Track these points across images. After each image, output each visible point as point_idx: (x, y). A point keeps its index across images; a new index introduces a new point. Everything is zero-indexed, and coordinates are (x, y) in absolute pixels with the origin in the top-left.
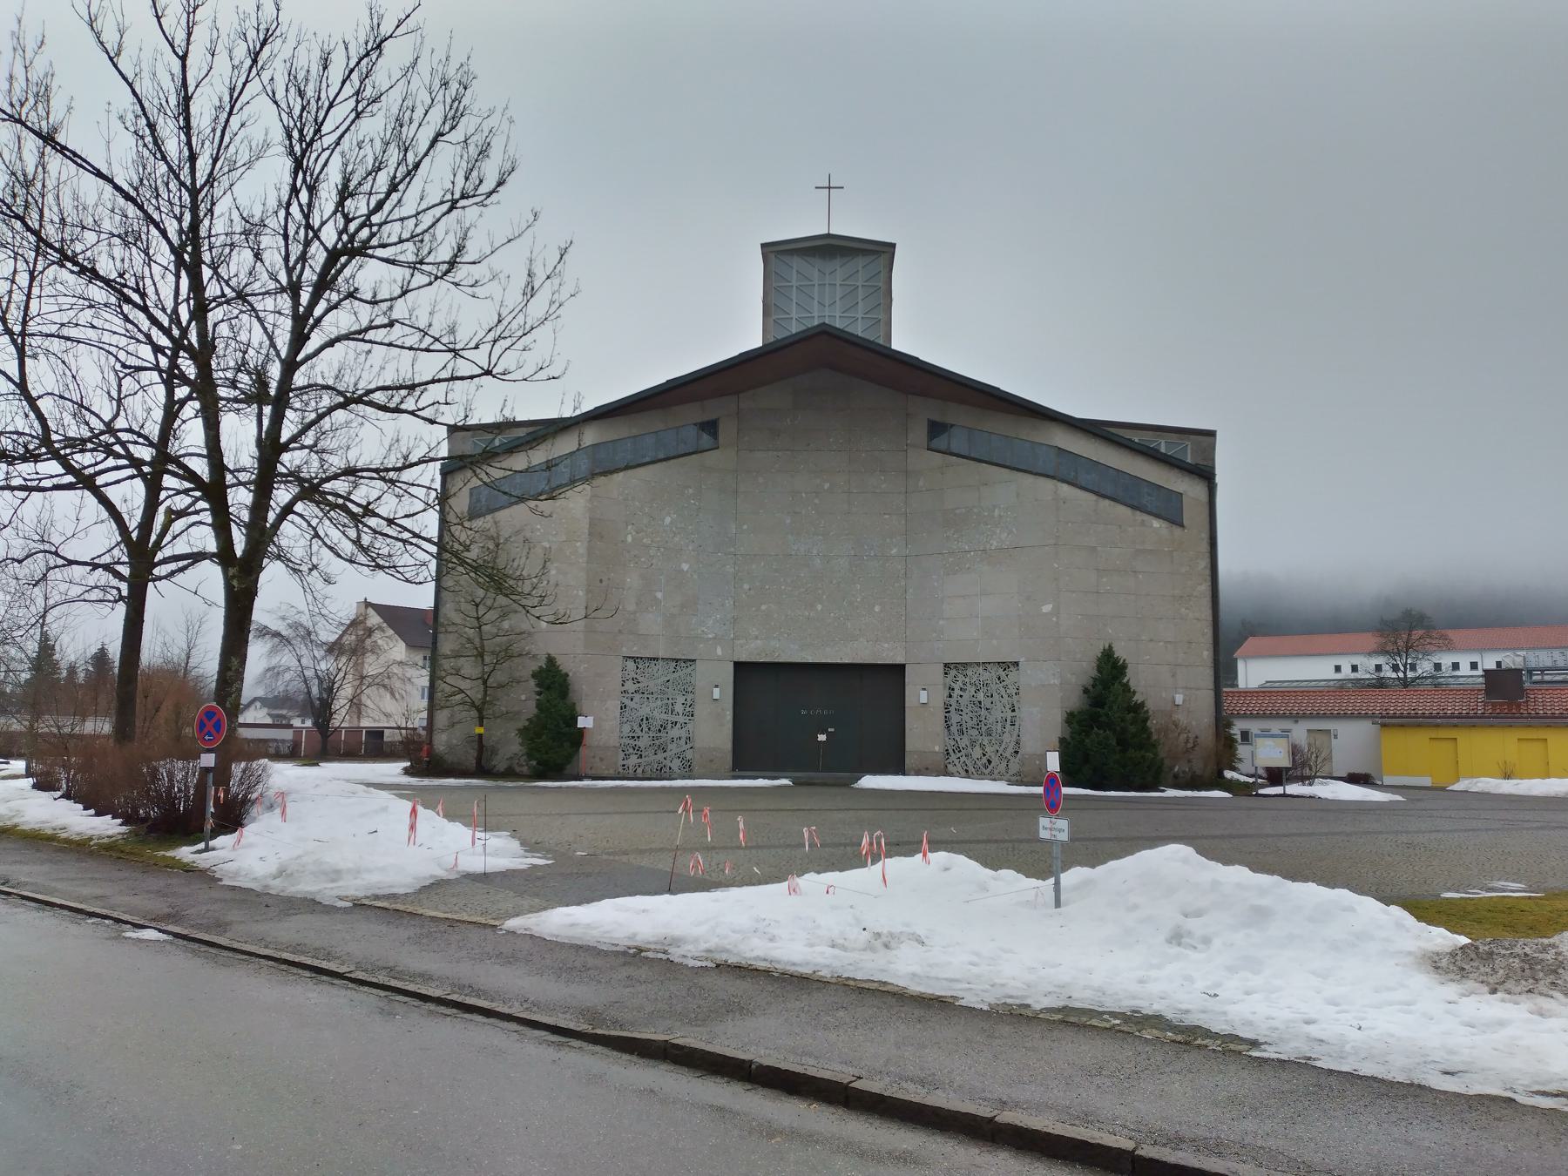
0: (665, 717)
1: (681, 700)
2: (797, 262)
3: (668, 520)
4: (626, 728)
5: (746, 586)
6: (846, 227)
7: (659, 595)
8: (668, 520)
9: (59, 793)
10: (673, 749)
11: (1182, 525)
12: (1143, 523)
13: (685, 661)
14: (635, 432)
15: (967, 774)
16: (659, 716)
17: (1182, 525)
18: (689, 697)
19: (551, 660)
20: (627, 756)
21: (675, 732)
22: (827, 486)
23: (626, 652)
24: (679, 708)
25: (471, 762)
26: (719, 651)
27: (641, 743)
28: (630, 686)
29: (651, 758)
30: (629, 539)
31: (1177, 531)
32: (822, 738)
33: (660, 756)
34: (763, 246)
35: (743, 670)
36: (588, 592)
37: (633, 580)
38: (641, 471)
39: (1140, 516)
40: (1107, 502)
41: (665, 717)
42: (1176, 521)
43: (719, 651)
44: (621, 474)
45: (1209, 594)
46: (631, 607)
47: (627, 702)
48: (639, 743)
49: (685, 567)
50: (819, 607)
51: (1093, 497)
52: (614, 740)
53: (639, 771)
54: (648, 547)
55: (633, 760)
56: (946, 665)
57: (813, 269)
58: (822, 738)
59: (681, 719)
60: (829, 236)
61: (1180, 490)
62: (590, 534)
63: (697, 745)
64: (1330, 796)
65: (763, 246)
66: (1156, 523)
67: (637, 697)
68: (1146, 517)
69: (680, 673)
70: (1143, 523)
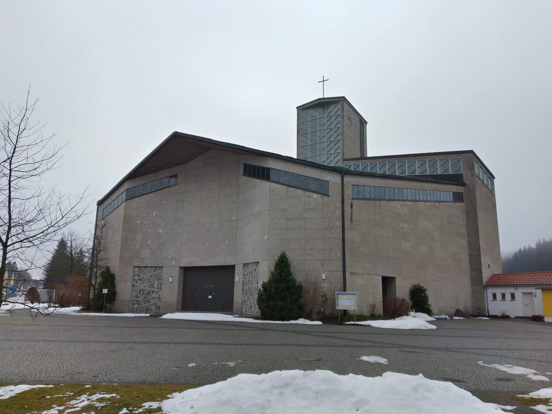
0: (150, 289)
1: (156, 282)
2: (310, 111)
3: (154, 214)
4: (134, 294)
5: (185, 237)
6: (329, 94)
7: (149, 242)
8: (154, 214)
9: (432, 319)
10: (153, 302)
11: (328, 196)
12: (309, 196)
13: (159, 267)
14: (143, 182)
15: (106, 313)
16: (148, 289)
17: (328, 196)
18: (160, 281)
19: (108, 269)
20: (134, 304)
21: (154, 295)
22: (212, 194)
23: (135, 264)
24: (156, 286)
25: (380, 309)
26: (173, 263)
27: (140, 299)
28: (136, 278)
29: (143, 305)
30: (139, 222)
31: (326, 198)
32: (210, 297)
33: (147, 304)
34: (297, 108)
35: (187, 271)
36: (122, 243)
37: (139, 237)
38: (144, 197)
39: (307, 193)
40: (292, 189)
41: (150, 289)
42: (325, 194)
43: (173, 263)
44: (137, 198)
45: (341, 226)
46: (138, 247)
47: (135, 284)
48: (139, 299)
49: (160, 231)
50: (208, 243)
51: (285, 187)
52: (128, 298)
53: (139, 310)
54: (146, 224)
55: (136, 306)
56: (244, 265)
57: (316, 113)
58: (210, 297)
59: (156, 290)
60: (323, 98)
61: (328, 179)
62: (124, 221)
63: (162, 300)
64: (408, 327)
65: (297, 108)
66: (315, 196)
67: (139, 282)
68: (311, 194)
69: (157, 272)
70: (309, 196)
